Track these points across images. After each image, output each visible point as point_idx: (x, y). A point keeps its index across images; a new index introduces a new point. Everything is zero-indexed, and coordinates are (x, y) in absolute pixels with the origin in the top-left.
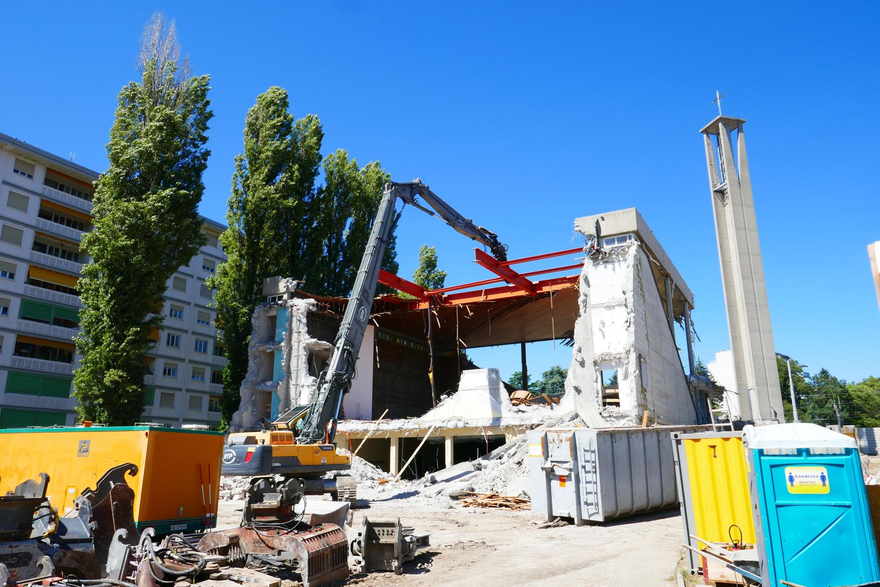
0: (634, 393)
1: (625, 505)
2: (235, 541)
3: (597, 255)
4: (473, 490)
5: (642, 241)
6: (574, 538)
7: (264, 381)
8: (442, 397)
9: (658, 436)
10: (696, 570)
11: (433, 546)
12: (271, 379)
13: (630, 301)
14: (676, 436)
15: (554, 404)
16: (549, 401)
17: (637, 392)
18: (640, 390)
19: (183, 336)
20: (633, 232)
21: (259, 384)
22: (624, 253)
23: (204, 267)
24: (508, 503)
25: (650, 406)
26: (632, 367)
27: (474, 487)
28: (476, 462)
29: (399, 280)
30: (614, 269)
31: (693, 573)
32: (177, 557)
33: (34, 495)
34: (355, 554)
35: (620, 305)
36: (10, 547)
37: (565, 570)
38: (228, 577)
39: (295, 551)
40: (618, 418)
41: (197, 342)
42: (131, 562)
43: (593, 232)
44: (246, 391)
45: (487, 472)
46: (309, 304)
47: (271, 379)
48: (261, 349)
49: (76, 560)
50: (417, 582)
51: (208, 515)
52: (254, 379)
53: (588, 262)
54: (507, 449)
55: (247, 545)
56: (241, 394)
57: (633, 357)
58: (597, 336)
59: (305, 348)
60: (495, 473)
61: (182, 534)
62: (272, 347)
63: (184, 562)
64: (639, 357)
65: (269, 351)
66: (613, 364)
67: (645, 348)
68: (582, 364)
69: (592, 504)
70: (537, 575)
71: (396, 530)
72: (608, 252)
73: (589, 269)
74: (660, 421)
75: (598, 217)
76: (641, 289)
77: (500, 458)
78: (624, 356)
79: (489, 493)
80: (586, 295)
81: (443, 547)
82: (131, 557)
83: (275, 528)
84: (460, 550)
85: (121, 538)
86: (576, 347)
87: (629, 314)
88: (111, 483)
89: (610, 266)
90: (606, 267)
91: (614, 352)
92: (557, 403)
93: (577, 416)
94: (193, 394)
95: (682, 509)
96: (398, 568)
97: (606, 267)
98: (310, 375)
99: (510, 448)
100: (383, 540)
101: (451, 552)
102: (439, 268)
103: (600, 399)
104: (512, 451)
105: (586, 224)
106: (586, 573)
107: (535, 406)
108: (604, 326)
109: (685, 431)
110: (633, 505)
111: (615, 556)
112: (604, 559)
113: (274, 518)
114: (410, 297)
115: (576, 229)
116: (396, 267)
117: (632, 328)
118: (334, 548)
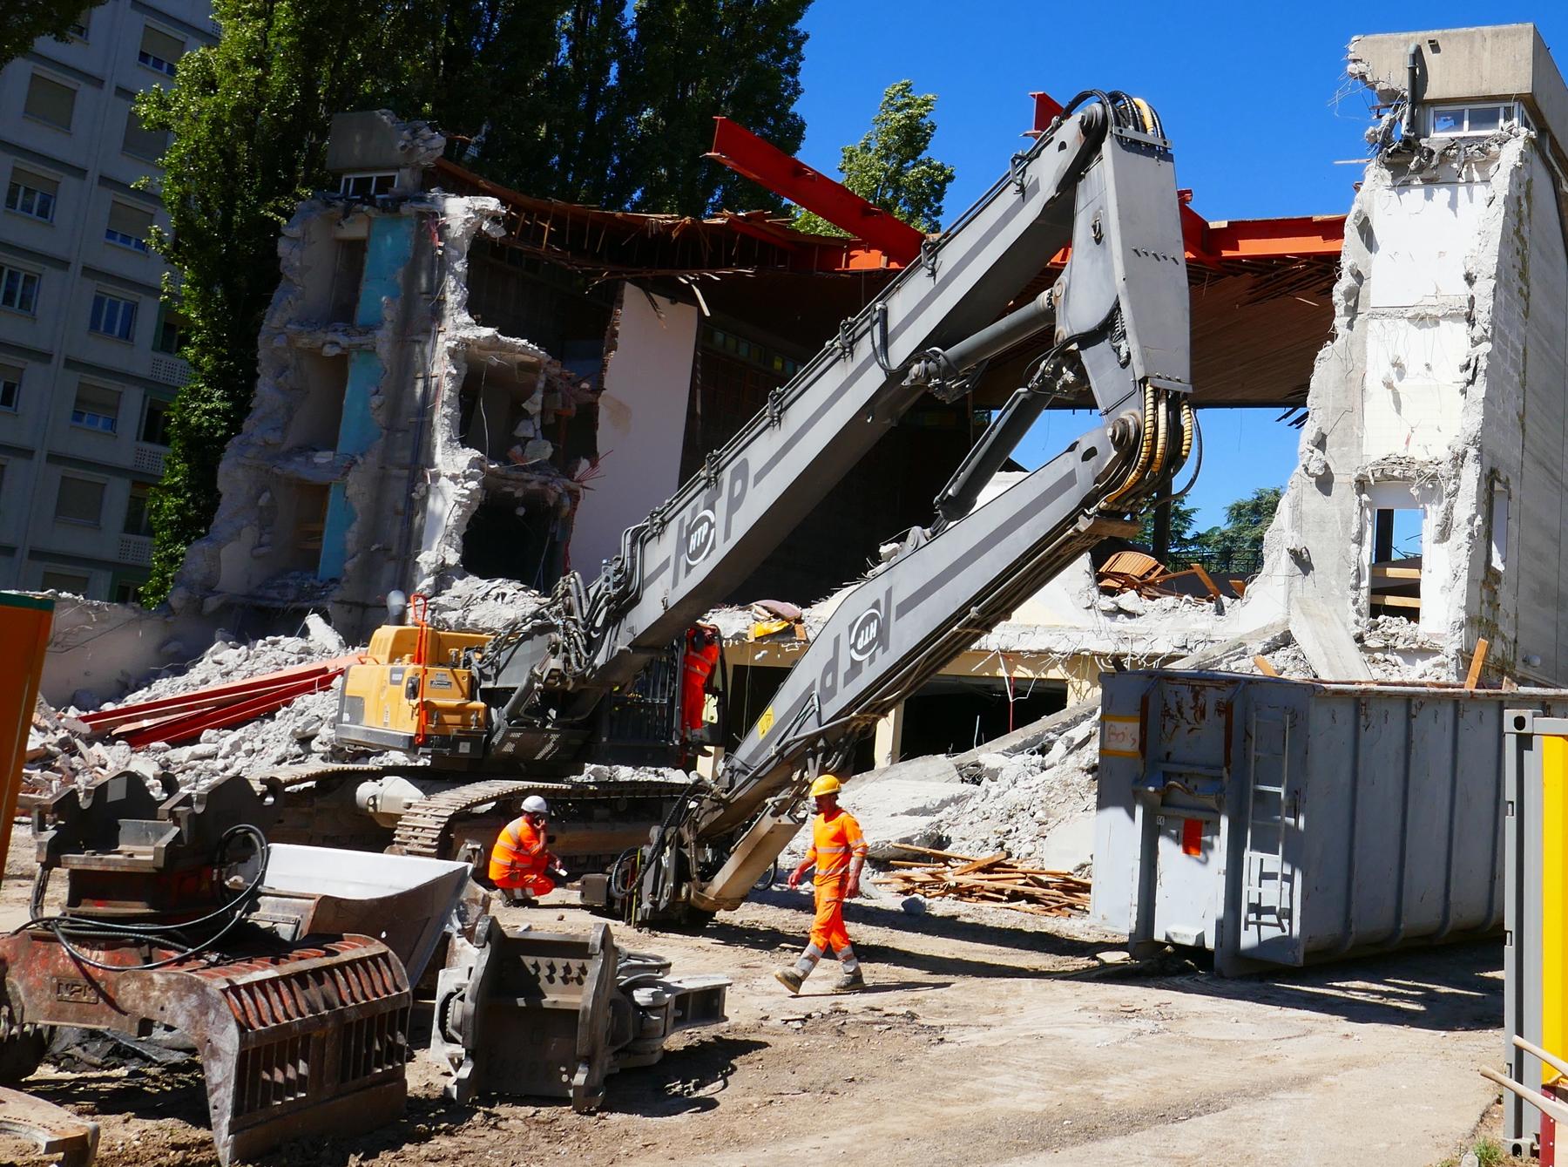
0: (1462, 584)
1: (1373, 919)
3: (1407, 160)
4: (942, 842)
5: (1543, 129)
6: (1199, 1015)
7: (306, 449)
8: (884, 550)
9: (1409, 717)
10: (1526, 1141)
11: (739, 1013)
12: (331, 445)
13: (1484, 307)
14: (1520, 723)
15: (1226, 600)
16: (1211, 586)
17: (1471, 581)
18: (1481, 575)
19: (51, 281)
20: (1520, 98)
21: (288, 456)
22: (1485, 156)
23: (144, 57)
24: (1038, 891)
25: (1505, 627)
26: (1466, 506)
27: (946, 832)
28: (965, 757)
29: (799, 168)
30: (1453, 204)
31: (1517, 1150)
34: (449, 1039)
35: (1452, 317)
37: (1129, 1122)
39: (194, 1023)
40: (1412, 654)
41: (98, 302)
43: (1400, 81)
44: (240, 473)
45: (994, 791)
46: (482, 214)
47: (331, 445)
48: (304, 342)
50: (638, 1142)
52: (272, 437)
53: (1376, 178)
54: (1067, 726)
55: (30, 992)
56: (222, 485)
57: (1471, 475)
58: (1377, 403)
59: (453, 353)
60: (1017, 795)
62: (344, 341)
64: (1490, 479)
65: (330, 351)
66: (1414, 491)
67: (1510, 452)
68: (1325, 483)
69: (1271, 910)
70: (1041, 1134)
71: (595, 967)
72: (1437, 149)
73: (1375, 194)
74: (1531, 674)
75: (1420, 37)
76: (1523, 275)
77: (1043, 751)
78: (1445, 469)
79: (987, 856)
80: (1359, 277)
81: (775, 1022)
83: (138, 943)
84: (827, 1038)
86: (1309, 431)
87: (1475, 343)
89: (1442, 194)
90: (1429, 196)
91: (1420, 456)
92: (1236, 594)
93: (1286, 640)
94: (72, 472)
95: (1509, 951)
96: (589, 1090)
97: (1429, 196)
98: (465, 443)
99: (1075, 722)
100: (556, 997)
101: (795, 1041)
102: (935, 152)
103: (1365, 593)
104: (1078, 733)
105: (1381, 58)
106: (1191, 1136)
107: (1169, 601)
108: (1401, 376)
109: (1546, 707)
110: (1398, 917)
111: (1301, 1082)
112: (1262, 1091)
113: (139, 908)
114: (822, 227)
115: (1351, 67)
116: (795, 132)
117: (1479, 390)
118: (352, 1017)
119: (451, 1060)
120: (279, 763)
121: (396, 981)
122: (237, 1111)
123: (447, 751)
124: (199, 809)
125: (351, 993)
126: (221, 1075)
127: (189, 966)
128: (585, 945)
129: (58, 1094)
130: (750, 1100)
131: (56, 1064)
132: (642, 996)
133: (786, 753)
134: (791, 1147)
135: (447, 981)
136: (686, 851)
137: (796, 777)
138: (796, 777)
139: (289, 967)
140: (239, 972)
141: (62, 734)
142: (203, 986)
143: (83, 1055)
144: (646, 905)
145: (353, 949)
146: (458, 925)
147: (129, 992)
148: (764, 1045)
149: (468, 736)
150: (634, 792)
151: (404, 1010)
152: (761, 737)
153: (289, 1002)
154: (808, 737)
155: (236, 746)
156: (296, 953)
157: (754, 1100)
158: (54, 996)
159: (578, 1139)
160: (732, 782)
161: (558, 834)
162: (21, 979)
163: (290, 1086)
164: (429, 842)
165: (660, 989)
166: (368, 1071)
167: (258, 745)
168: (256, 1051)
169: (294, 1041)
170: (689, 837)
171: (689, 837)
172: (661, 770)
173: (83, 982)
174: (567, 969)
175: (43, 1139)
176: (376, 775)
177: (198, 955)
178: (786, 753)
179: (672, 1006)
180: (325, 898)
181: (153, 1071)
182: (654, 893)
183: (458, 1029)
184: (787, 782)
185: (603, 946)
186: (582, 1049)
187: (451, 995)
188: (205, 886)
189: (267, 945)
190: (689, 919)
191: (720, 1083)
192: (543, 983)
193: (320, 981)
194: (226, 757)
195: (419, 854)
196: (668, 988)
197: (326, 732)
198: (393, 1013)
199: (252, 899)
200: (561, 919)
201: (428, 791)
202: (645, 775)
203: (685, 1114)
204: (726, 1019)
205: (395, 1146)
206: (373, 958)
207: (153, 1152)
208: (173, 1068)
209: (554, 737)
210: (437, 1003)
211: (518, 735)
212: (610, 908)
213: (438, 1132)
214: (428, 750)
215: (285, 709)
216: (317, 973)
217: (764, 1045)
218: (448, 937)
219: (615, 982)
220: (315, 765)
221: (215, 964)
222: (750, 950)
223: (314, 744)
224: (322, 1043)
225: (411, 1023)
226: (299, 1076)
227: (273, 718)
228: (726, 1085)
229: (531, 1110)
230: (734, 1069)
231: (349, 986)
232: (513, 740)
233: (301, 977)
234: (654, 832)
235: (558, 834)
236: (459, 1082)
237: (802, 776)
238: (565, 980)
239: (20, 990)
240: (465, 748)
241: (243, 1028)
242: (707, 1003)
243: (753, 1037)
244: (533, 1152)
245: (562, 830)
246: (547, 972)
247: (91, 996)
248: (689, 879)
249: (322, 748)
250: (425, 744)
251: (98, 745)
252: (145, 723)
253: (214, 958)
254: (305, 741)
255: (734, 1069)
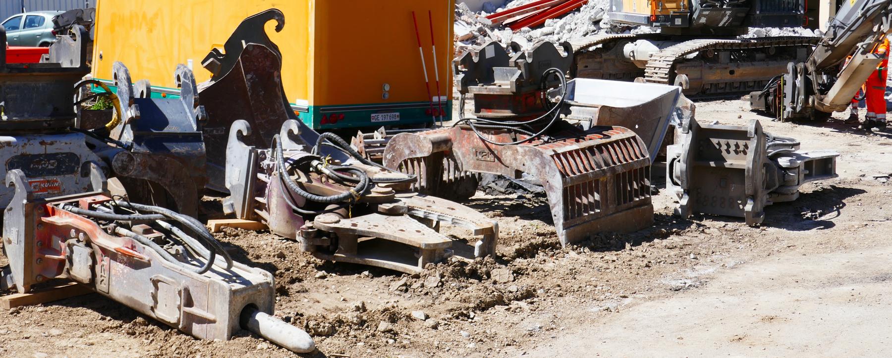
2: (444, 148)
32: (327, 172)
33: (71, 62)
34: (676, 184)
36: (42, 143)
38: (410, 212)
42: (260, 176)
49: (151, 168)
50: (785, 244)
51: (435, 99)
61: (382, 129)
63: (340, 181)
71: (752, 144)
81: (869, 178)
82: (258, 168)
83: (509, 131)
85: (290, 134)
88: (243, 42)
96: (755, 214)
100: (732, 161)
113: (507, 113)
118: (620, 170)
119: (678, 195)
120: (585, 35)
121: (642, 152)
122: (566, 218)
123: (668, 24)
124: (530, 61)
125: (618, 158)
126: (556, 199)
127: (534, 143)
128: (746, 132)
129: (484, 207)
130: (853, 223)
131: (485, 191)
132: (783, 162)
133: (868, 14)
134: (878, 252)
135: (672, 152)
136: (810, 77)
137: (875, 29)
138: (875, 29)
139: (584, 144)
140: (559, 146)
141: (479, 26)
142: (541, 154)
143: (496, 187)
144: (789, 109)
145: (619, 134)
146: (678, 121)
147: (507, 156)
148: (863, 191)
149: (681, 16)
150: (779, 43)
151: (647, 168)
152: (852, 5)
153: (586, 162)
154: (882, 4)
155: (562, 27)
156: (589, 136)
157: (856, 223)
158: (475, 158)
159: (750, 241)
160: (835, 34)
161: (735, 69)
162: (459, 149)
163: (591, 206)
164: (663, 76)
165: (794, 158)
166: (631, 199)
167: (573, 27)
168: (572, 187)
169: (590, 183)
170: (811, 69)
171: (811, 69)
172: (796, 29)
173: (487, 151)
174: (737, 146)
175: (473, 228)
176: (633, 40)
177: (539, 137)
178: (868, 14)
179: (802, 168)
180: (604, 107)
181: (529, 196)
182: (793, 102)
183: (678, 178)
184: (870, 33)
185: (756, 132)
186: (749, 191)
187: (674, 159)
188: (538, 101)
189: (576, 132)
190: (817, 117)
191: (836, 213)
192: (724, 154)
193: (601, 152)
194: (558, 34)
195: (659, 82)
196: (799, 157)
197: (606, 18)
198: (641, 169)
199: (565, 108)
200: (740, 117)
201: (661, 47)
202: (787, 32)
203: (814, 230)
204: (837, 176)
205: (649, 239)
206: (628, 139)
207: (529, 237)
208: (538, 195)
209: (728, 13)
210: (668, 163)
211: (707, 13)
212: (771, 110)
213: (672, 233)
214: (658, 24)
215: (584, 6)
216: (599, 147)
217: (863, 191)
218: (672, 128)
219: (765, 152)
220: (603, 35)
221: (547, 142)
222: (854, 135)
223: (601, 24)
224: (605, 184)
225: (657, 173)
226: (595, 201)
227: (579, 10)
228: (839, 214)
229: (722, 224)
230: (844, 205)
231: (617, 154)
232: (705, 16)
233: (591, 149)
234: (790, 66)
235: (735, 69)
236: (682, 207)
237: (879, 28)
238: (737, 152)
239: (460, 154)
240: (678, 22)
241: (564, 175)
242: (825, 166)
243: (855, 187)
244: (724, 247)
245: (738, 66)
246: (726, 147)
247: (491, 158)
248: (813, 93)
249: (605, 26)
250: (657, 21)
251: (496, 30)
252: (518, 18)
253: (546, 139)
254: (596, 23)
255: (844, 205)
